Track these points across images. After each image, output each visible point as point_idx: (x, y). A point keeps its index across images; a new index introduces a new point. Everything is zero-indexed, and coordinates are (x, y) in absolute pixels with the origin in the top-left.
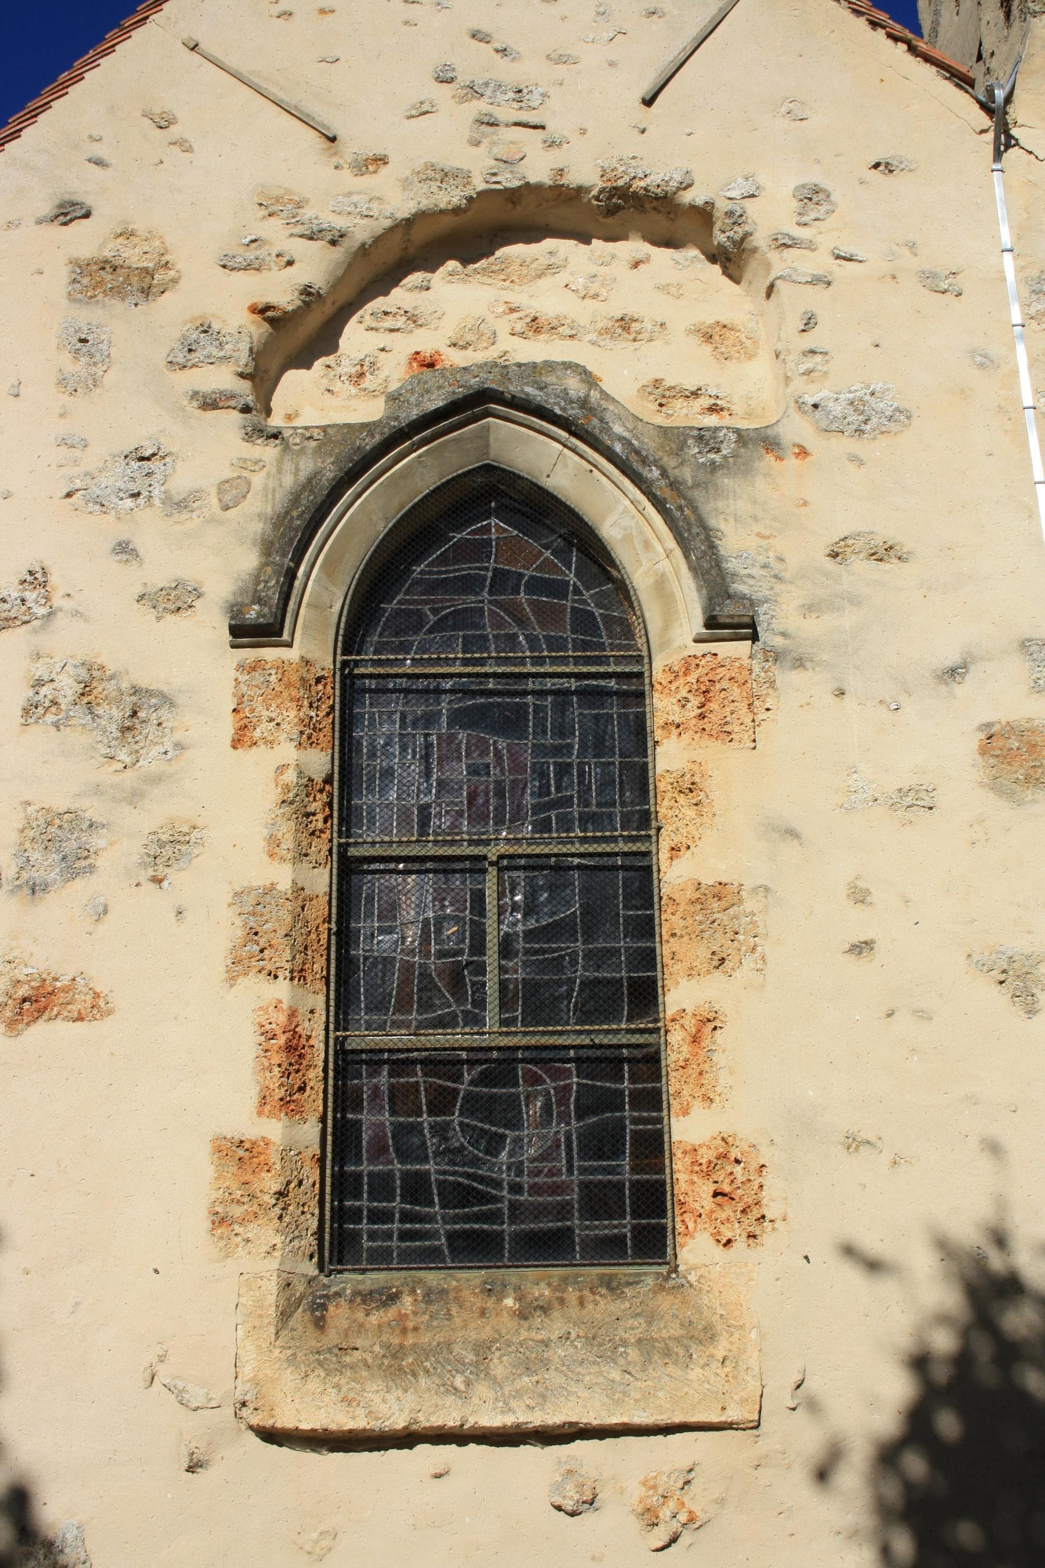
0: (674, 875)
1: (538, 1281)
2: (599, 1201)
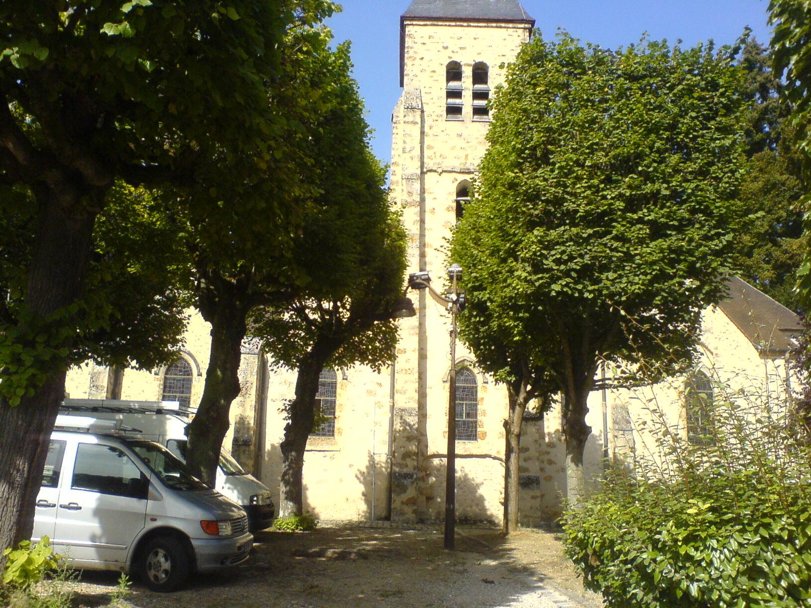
0: (337, 403)
1: (323, 438)
2: (329, 431)
